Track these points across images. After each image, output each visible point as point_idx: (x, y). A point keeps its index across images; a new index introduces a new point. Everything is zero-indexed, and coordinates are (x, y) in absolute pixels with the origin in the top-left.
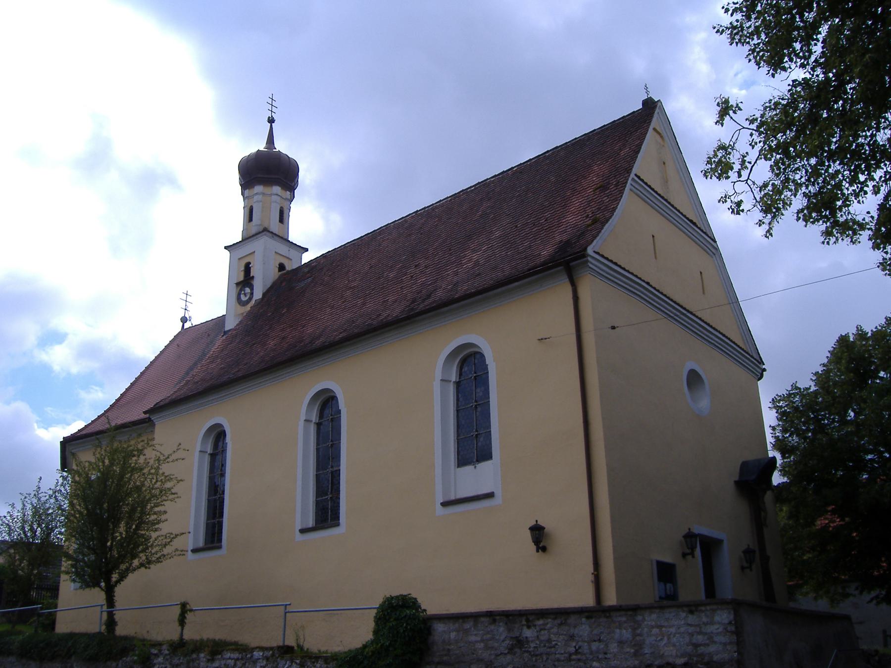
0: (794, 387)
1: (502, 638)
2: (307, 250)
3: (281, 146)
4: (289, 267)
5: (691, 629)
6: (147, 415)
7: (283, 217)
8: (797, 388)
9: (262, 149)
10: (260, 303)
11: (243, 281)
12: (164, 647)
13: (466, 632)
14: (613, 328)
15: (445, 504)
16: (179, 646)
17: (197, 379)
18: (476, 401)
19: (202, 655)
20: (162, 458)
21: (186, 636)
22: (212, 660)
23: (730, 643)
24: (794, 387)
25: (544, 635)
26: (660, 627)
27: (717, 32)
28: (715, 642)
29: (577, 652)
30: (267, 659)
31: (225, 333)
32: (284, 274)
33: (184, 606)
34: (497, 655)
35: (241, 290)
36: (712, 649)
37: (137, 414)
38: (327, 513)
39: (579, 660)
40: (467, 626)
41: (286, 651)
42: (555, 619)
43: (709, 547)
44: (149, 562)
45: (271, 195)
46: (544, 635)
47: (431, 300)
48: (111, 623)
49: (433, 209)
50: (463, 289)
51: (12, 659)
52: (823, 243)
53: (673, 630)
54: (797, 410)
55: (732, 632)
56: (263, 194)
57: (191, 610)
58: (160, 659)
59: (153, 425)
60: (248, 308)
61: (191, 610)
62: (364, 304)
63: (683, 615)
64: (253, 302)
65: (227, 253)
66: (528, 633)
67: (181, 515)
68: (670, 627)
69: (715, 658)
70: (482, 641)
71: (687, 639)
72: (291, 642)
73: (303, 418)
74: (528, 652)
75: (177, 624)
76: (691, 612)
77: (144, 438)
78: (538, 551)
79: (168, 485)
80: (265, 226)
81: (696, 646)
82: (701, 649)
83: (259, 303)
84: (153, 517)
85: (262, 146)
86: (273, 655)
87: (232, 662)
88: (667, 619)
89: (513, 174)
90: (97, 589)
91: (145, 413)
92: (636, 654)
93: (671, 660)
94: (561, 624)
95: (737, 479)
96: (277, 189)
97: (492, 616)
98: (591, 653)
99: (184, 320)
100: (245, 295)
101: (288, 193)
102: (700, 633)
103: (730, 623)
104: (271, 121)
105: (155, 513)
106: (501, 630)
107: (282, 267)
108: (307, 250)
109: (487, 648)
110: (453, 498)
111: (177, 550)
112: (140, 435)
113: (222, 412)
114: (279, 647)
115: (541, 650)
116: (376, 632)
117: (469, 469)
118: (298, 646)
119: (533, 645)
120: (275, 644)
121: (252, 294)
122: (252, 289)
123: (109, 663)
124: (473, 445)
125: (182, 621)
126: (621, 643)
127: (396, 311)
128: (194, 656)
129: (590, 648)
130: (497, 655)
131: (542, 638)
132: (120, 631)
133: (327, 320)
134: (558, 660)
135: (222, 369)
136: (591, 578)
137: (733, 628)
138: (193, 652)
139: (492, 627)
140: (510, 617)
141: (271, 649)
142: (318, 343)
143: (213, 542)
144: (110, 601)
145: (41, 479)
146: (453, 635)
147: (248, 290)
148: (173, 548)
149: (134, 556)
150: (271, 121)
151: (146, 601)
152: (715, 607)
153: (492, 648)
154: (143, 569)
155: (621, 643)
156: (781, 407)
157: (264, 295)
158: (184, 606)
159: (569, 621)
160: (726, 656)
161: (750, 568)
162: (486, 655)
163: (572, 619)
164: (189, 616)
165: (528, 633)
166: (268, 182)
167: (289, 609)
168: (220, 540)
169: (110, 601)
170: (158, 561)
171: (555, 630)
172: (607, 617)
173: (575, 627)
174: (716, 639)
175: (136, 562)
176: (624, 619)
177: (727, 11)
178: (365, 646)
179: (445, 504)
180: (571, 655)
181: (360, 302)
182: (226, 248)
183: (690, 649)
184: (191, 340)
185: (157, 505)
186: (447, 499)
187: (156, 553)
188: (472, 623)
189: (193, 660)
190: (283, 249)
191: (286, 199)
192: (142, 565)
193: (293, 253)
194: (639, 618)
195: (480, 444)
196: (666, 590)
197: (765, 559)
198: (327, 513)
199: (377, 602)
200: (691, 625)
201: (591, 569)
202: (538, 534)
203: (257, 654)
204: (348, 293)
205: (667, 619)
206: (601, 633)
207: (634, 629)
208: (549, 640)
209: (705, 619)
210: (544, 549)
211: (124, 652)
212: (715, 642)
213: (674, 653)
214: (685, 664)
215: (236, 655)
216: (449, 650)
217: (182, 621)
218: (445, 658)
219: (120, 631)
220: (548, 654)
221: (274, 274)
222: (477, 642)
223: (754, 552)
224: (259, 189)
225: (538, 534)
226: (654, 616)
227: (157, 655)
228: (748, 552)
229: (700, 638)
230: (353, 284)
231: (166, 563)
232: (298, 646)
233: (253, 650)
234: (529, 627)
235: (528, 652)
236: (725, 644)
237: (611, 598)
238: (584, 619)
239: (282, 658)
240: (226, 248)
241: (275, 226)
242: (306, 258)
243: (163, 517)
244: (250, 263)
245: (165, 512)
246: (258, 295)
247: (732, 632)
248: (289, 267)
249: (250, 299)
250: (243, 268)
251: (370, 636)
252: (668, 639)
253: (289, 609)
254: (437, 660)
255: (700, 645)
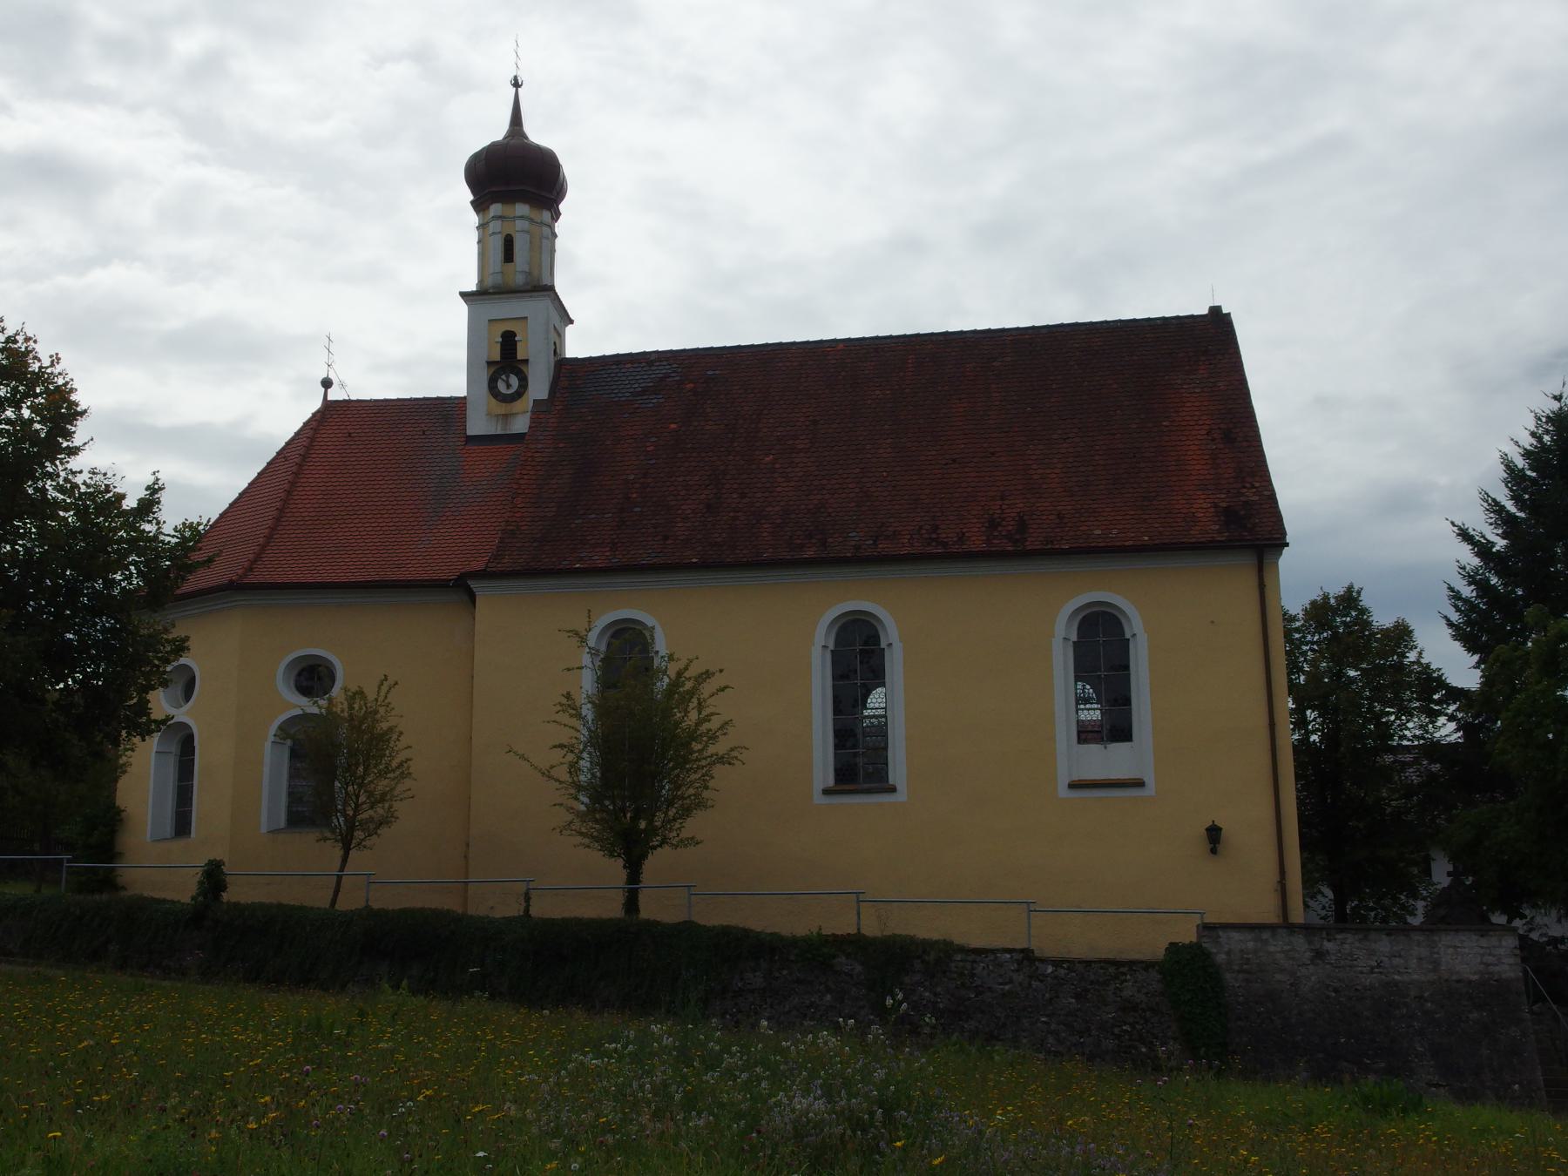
3: (537, 133)
15: (1074, 786)
21: (650, 909)
29: (1379, 966)
45: (515, 218)
56: (532, 220)
63: (1474, 937)
66: (1328, 945)
81: (1488, 965)
82: (1492, 969)
96: (522, 209)
117: (1094, 748)
120: (1018, 946)
132: (646, 913)
146: (1251, 945)
165: (1328, 945)
174: (1505, 960)
179: (1074, 786)
219: (646, 913)
229: (1490, 959)
233: (1043, 961)
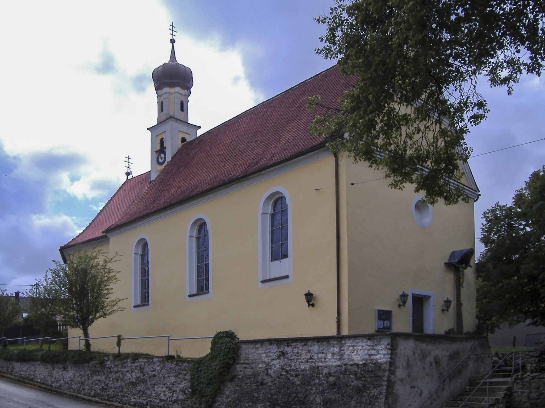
0: (497, 205)
1: (275, 351)
2: (200, 127)
3: (181, 60)
4: (188, 139)
5: (368, 348)
6: (104, 234)
7: (183, 107)
8: (498, 206)
9: (167, 62)
10: (170, 164)
11: (159, 150)
12: (111, 357)
13: (257, 349)
14: (353, 184)
15: (263, 282)
16: (118, 356)
17: (132, 212)
18: (282, 225)
19: (129, 360)
20: (107, 260)
21: (122, 351)
22: (134, 363)
23: (387, 354)
24: (497, 205)
25: (296, 351)
26: (353, 346)
27: (317, 52)
28: (380, 354)
29: (311, 358)
30: (160, 362)
31: (151, 182)
32: (186, 144)
33: (119, 337)
34: (272, 360)
35: (159, 156)
36: (378, 356)
37: (98, 233)
38: (203, 288)
39: (312, 362)
40: (257, 346)
41: (170, 358)
42: (301, 342)
43: (420, 301)
44: (105, 314)
46: (296, 351)
47: (198, 189)
48: (88, 345)
49: (273, 101)
50: (277, 158)
51: (38, 363)
52: (469, 132)
53: (360, 348)
54: (497, 219)
55: (389, 349)
57: (123, 339)
58: (109, 362)
59: (109, 240)
60: (163, 166)
61: (123, 339)
62: (224, 166)
63: (365, 340)
64: (166, 163)
65: (149, 133)
67: (122, 289)
68: (359, 346)
69: (379, 361)
70: (265, 353)
71: (366, 352)
72: (173, 353)
73: (188, 234)
74: (287, 358)
75: (116, 346)
76: (370, 339)
77: (96, 250)
78: (309, 306)
79: (111, 275)
80: (173, 113)
81: (370, 355)
82: (372, 357)
83: (169, 164)
84: (105, 292)
85: (166, 59)
86: (163, 360)
87: (143, 364)
88: (357, 343)
89: (321, 77)
90: (78, 328)
91: (103, 232)
92: (340, 359)
93: (357, 362)
94: (304, 345)
95: (447, 261)
96: (178, 89)
97: (270, 341)
98: (318, 358)
99: (128, 174)
100: (161, 158)
101: (186, 91)
102: (372, 349)
103: (388, 344)
104: (173, 41)
105: (106, 289)
106: (274, 349)
107: (183, 140)
108: (200, 127)
109: (267, 356)
110: (268, 278)
111: (120, 308)
112: (95, 248)
113: (147, 231)
114: (165, 356)
115: (293, 357)
116: (212, 349)
117: (277, 262)
118: (178, 355)
119: (289, 355)
121: (165, 158)
122: (165, 155)
123: (84, 364)
124: (279, 250)
125: (119, 344)
126: (333, 354)
127: (238, 173)
128: (125, 361)
129: (318, 356)
130: (272, 360)
131: (294, 352)
132: (92, 349)
133: (204, 176)
134: (302, 362)
135: (146, 206)
136: (336, 320)
137: (389, 347)
138: (124, 359)
139: (270, 346)
140: (278, 342)
141: (162, 357)
142: (196, 191)
143: (145, 301)
144: (86, 334)
145: (510, 93)
147: (163, 155)
148: (118, 307)
149: (97, 312)
150: (173, 41)
151: (102, 334)
152: (381, 337)
153: (270, 356)
154: (102, 318)
155: (333, 354)
156: (489, 217)
157: (173, 158)
158: (119, 337)
159: (308, 344)
160: (384, 360)
161: (447, 310)
162: (266, 360)
163: (310, 343)
164: (122, 341)
166: (171, 85)
167: (171, 338)
168: (207, 288)
169: (86, 334)
170: (110, 313)
171: (301, 348)
172: (327, 342)
173: (311, 347)
175: (98, 315)
176: (336, 342)
177: (322, 40)
178: (207, 356)
179: (263, 282)
180: (308, 359)
181: (223, 164)
182: (148, 129)
183: (367, 357)
184: (132, 183)
185: (106, 286)
186: (264, 279)
187: (109, 310)
188: (260, 345)
189: (125, 363)
190: (184, 128)
191: (185, 95)
192: (101, 316)
193: (191, 130)
194: (343, 342)
195: (283, 249)
196: (384, 324)
197: (459, 305)
198: (203, 288)
199: (213, 335)
200: (369, 346)
201: (336, 315)
202: (309, 297)
203: (155, 360)
204: (217, 159)
205: (357, 343)
206: (324, 349)
207: (340, 347)
208: (298, 353)
209: (376, 343)
210: (313, 305)
211: (91, 359)
212: (380, 354)
213: (359, 359)
214: (364, 364)
215: (145, 360)
216: (248, 357)
217: (119, 344)
218: (246, 361)
220: (297, 359)
221: (179, 144)
222: (262, 354)
223: (450, 302)
224: (166, 89)
225: (309, 297)
226: (351, 341)
227: (107, 361)
228: (448, 303)
230: (221, 153)
231: (114, 315)
232: (178, 355)
234: (288, 346)
235: (287, 358)
236: (384, 354)
237: (345, 332)
238: (316, 343)
239: (167, 362)
240: (148, 129)
241: (179, 115)
242: (200, 133)
243: (111, 291)
244: (163, 138)
245: (112, 289)
246: (169, 159)
247: (389, 349)
248: (188, 139)
249: (165, 161)
250: (159, 142)
251: (209, 351)
252: (357, 352)
253: (171, 338)
254: (242, 362)
255: (373, 355)
